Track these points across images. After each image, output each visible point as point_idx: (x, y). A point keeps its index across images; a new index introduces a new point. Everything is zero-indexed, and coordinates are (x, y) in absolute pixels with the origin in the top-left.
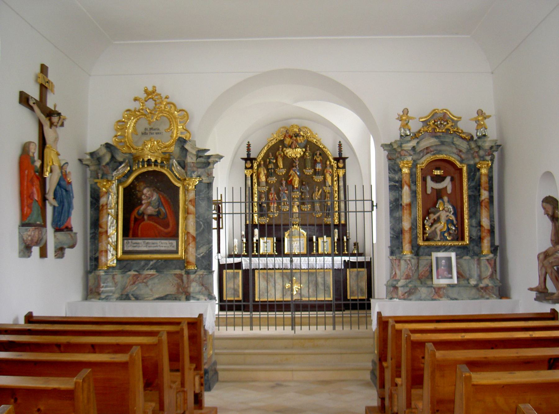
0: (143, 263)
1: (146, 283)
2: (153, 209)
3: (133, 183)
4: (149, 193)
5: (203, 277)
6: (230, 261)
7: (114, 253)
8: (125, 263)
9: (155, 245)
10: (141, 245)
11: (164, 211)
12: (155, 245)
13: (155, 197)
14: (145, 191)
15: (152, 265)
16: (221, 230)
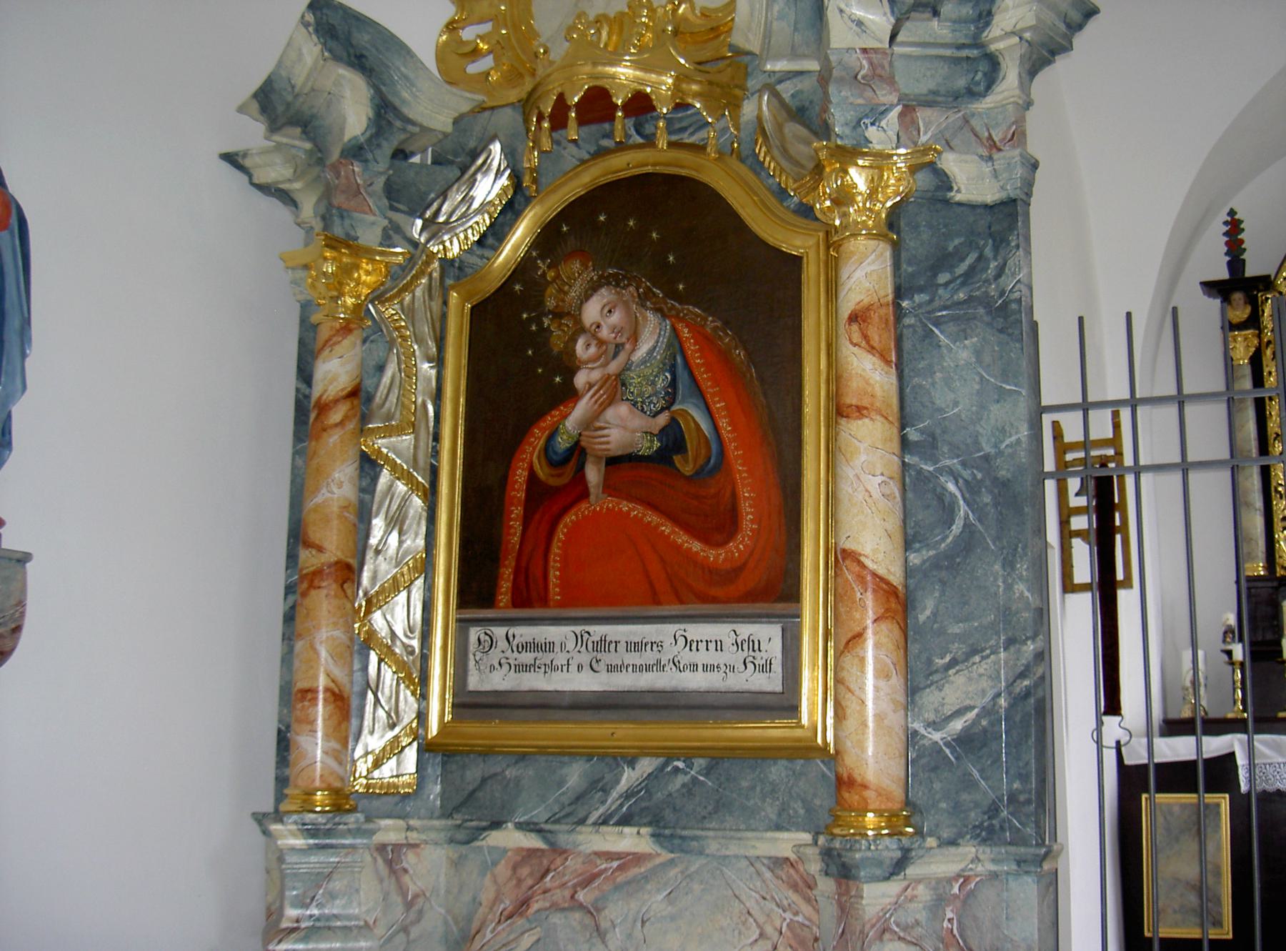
0: (575, 775)
1: (592, 912)
2: (639, 422)
3: (523, 269)
4: (616, 318)
5: (968, 898)
6: (1179, 749)
7: (409, 705)
8: (474, 773)
9: (649, 657)
10: (560, 659)
11: (705, 426)
12: (649, 657)
13: (652, 337)
14: (592, 311)
15: (628, 795)
16: (1122, 595)
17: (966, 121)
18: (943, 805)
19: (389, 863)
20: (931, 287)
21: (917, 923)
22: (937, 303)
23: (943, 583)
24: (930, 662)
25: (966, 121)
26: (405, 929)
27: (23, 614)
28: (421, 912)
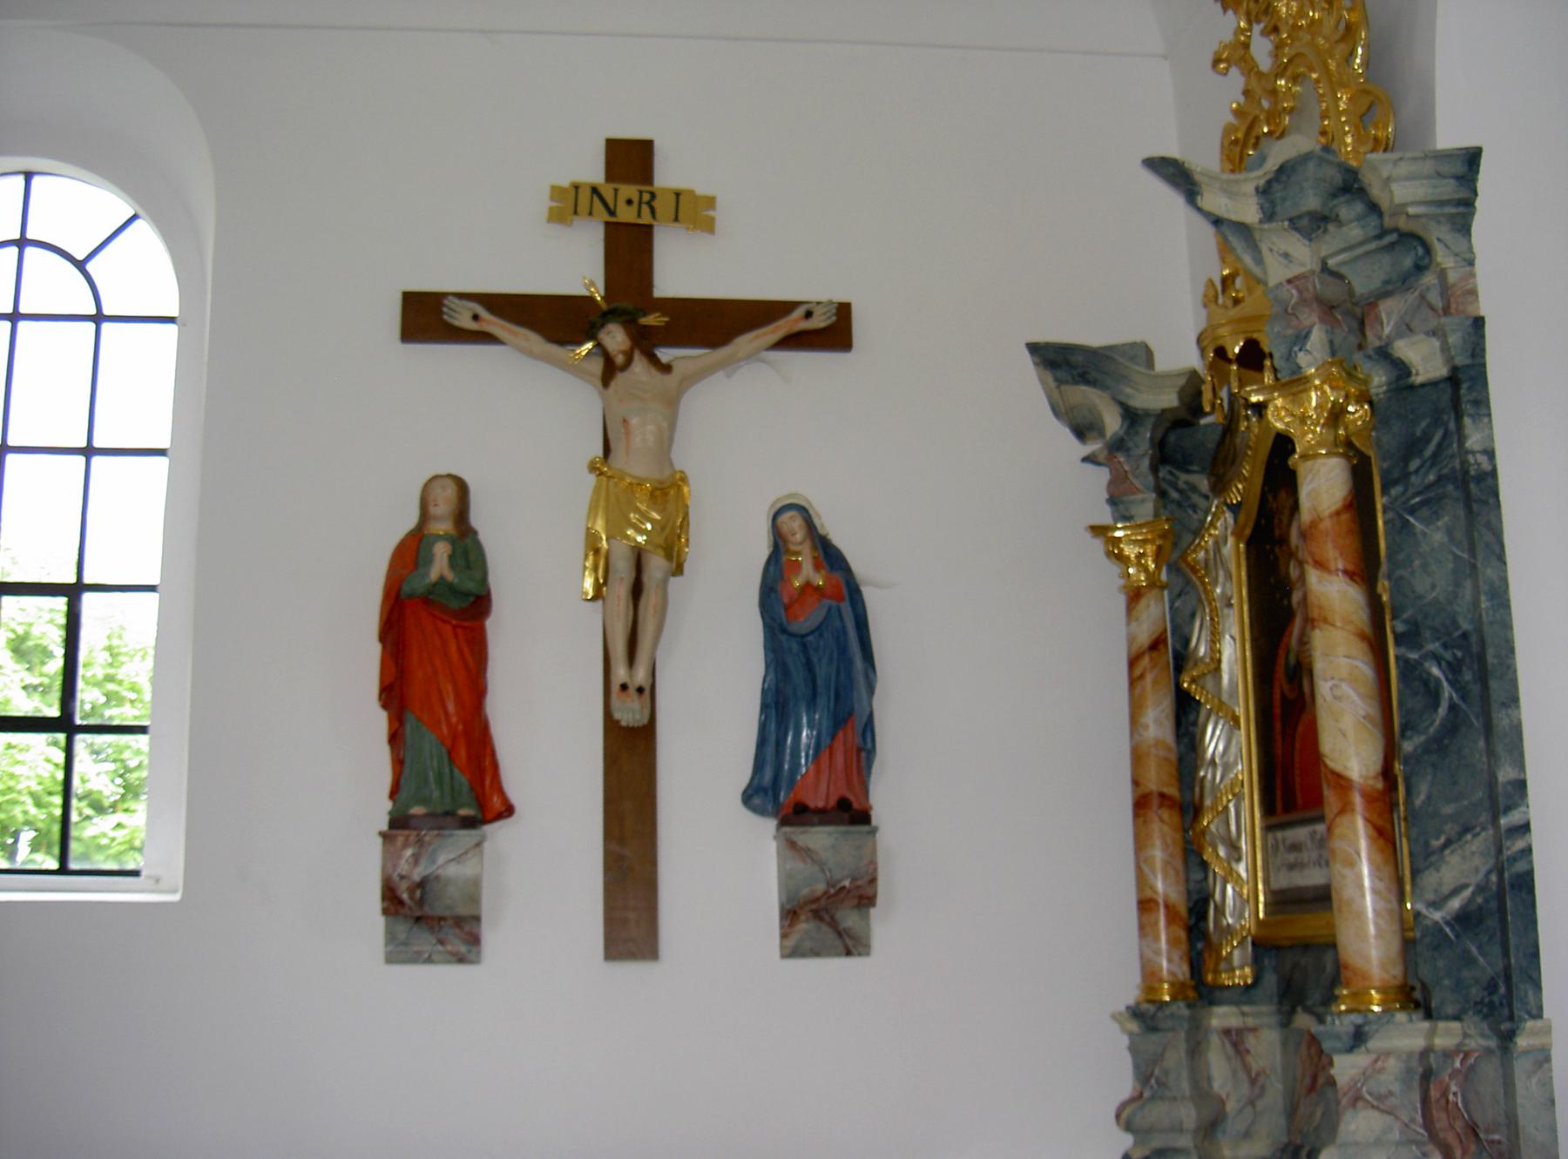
17: (1422, 297)
18: (1446, 982)
19: (1235, 1045)
20: (1406, 476)
21: (1391, 1093)
22: (1411, 491)
23: (1434, 766)
24: (1427, 844)
25: (1422, 297)
26: (1252, 1103)
27: (875, 870)
28: (1263, 1088)
